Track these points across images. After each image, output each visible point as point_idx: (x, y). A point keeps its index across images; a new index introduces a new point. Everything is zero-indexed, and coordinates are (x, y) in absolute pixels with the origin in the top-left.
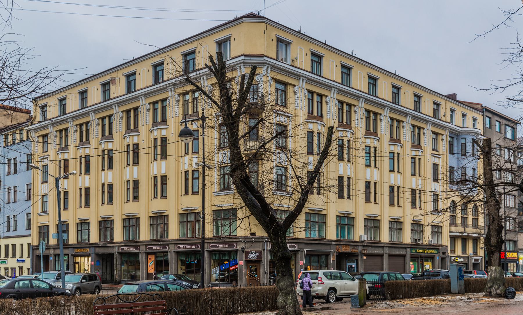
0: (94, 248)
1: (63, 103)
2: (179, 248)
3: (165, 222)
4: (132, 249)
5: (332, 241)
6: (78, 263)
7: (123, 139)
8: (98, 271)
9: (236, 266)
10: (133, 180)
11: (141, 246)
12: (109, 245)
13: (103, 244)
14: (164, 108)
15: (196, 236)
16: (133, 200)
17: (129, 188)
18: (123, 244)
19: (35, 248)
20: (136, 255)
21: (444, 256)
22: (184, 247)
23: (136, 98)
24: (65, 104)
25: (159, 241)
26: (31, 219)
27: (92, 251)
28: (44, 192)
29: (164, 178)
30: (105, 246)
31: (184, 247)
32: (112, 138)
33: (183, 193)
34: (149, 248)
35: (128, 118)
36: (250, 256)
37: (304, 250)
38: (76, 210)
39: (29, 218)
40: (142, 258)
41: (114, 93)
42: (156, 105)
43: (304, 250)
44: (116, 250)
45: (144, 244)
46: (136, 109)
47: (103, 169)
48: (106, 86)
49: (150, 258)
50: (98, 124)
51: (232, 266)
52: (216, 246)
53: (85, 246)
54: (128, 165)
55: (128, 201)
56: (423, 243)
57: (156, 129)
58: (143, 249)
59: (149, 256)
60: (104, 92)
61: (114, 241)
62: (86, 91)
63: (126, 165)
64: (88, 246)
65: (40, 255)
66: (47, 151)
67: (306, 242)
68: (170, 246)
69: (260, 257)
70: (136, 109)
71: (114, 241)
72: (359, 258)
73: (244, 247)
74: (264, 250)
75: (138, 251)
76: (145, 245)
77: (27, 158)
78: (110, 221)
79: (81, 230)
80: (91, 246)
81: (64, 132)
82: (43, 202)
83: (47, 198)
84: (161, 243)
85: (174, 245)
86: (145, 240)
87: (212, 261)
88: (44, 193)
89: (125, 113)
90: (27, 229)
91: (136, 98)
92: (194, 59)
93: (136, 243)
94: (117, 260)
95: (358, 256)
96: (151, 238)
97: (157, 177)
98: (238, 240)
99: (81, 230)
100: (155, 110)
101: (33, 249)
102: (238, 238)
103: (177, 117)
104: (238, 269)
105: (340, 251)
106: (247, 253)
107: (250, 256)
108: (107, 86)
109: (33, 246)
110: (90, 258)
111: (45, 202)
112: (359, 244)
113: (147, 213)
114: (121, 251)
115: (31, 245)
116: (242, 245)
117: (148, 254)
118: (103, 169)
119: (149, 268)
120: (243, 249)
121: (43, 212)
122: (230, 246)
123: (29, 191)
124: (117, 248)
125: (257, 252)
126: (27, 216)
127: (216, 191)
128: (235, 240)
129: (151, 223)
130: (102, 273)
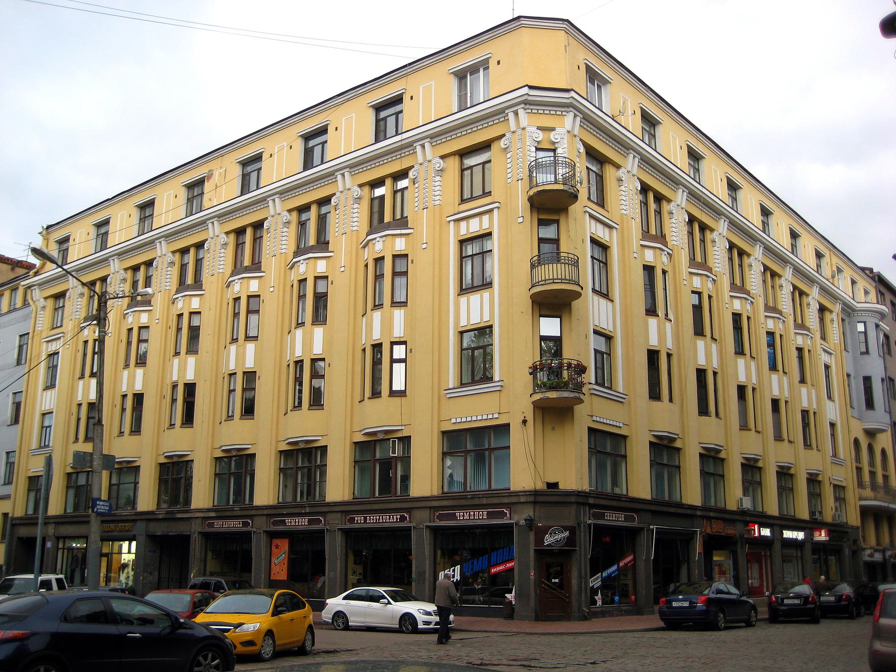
0: (145, 522)
1: (65, 246)
2: (352, 520)
3: (297, 464)
4: (234, 525)
5: (695, 508)
6: (106, 555)
7: (171, 305)
8: (151, 573)
9: (509, 565)
10: (244, 373)
11: (256, 519)
12: (179, 516)
13: (168, 513)
14: (322, 220)
15: (314, 498)
16: (242, 415)
17: (234, 390)
18: (213, 514)
19: (18, 522)
20: (245, 537)
21: (855, 548)
22: (365, 518)
23: (262, 201)
24: (67, 249)
25: (303, 507)
26: (14, 463)
27: (140, 528)
28: (47, 408)
29: (139, 398)
30: (170, 518)
31: (365, 518)
32: (200, 288)
33: (368, 393)
34: (275, 523)
35: (239, 245)
36: (548, 540)
37: (651, 527)
38: (213, 426)
39: (11, 460)
40: (258, 545)
41: (210, 200)
42: (186, 256)
43: (651, 527)
44: (195, 528)
45: (266, 512)
46: (258, 226)
47: (127, 366)
48: (196, 187)
49: (277, 546)
50: (172, 263)
51: (497, 565)
52: (454, 517)
53: (125, 518)
54: (177, 354)
55: (230, 417)
56: (794, 516)
57: (182, 297)
58: (259, 526)
59: (276, 542)
60: (142, 220)
61: (193, 506)
62: (151, 204)
63: (172, 353)
64: (131, 518)
65: (35, 538)
66: (61, 326)
67: (653, 508)
68: (330, 516)
69: (571, 541)
70: (258, 226)
71: (193, 506)
72: (739, 546)
73: (533, 518)
74: (579, 525)
75: (249, 529)
76: (267, 515)
77: (20, 341)
78: (185, 463)
79: (118, 485)
80: (138, 518)
81: (249, 232)
82: (43, 427)
83: (51, 418)
84: (308, 510)
85: (339, 515)
86: (266, 503)
87: (439, 553)
88: (47, 407)
89: (232, 237)
90: (5, 484)
91: (262, 201)
92: (259, 169)
93: (251, 512)
94: (196, 547)
95: (735, 543)
96: (446, 490)
97: (302, 361)
98: (514, 500)
99: (118, 485)
100: (302, 225)
101: (13, 525)
102: (517, 494)
103: (437, 208)
104: (516, 571)
105: (709, 531)
106: (540, 534)
107: (548, 540)
108: (196, 190)
109: (13, 519)
110: (134, 544)
111: (47, 427)
112: (737, 517)
113: (274, 443)
114: (208, 530)
115: (10, 515)
116: (527, 512)
117: (273, 535)
118: (127, 366)
119: (275, 569)
120: (530, 522)
121: (41, 447)
122: (490, 515)
123: (17, 406)
124: (199, 521)
125: (565, 528)
126: (8, 458)
127: (451, 386)
128: (506, 500)
129: (282, 466)
130: (159, 578)
